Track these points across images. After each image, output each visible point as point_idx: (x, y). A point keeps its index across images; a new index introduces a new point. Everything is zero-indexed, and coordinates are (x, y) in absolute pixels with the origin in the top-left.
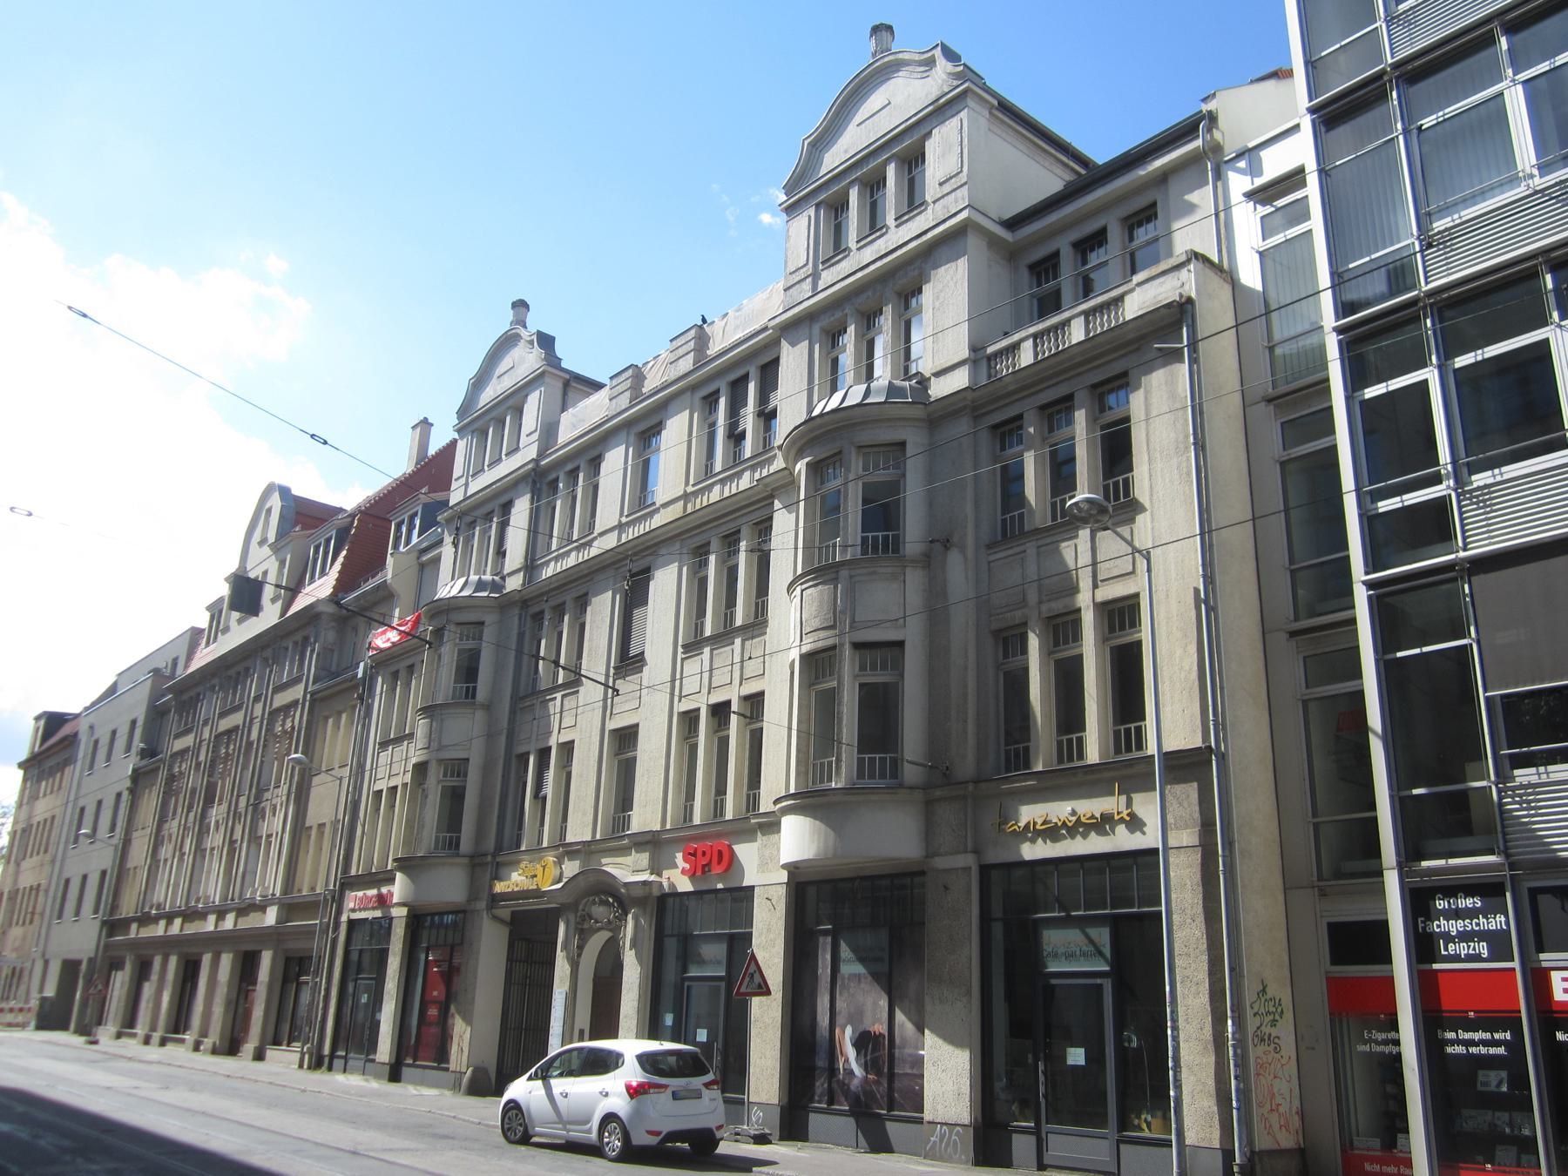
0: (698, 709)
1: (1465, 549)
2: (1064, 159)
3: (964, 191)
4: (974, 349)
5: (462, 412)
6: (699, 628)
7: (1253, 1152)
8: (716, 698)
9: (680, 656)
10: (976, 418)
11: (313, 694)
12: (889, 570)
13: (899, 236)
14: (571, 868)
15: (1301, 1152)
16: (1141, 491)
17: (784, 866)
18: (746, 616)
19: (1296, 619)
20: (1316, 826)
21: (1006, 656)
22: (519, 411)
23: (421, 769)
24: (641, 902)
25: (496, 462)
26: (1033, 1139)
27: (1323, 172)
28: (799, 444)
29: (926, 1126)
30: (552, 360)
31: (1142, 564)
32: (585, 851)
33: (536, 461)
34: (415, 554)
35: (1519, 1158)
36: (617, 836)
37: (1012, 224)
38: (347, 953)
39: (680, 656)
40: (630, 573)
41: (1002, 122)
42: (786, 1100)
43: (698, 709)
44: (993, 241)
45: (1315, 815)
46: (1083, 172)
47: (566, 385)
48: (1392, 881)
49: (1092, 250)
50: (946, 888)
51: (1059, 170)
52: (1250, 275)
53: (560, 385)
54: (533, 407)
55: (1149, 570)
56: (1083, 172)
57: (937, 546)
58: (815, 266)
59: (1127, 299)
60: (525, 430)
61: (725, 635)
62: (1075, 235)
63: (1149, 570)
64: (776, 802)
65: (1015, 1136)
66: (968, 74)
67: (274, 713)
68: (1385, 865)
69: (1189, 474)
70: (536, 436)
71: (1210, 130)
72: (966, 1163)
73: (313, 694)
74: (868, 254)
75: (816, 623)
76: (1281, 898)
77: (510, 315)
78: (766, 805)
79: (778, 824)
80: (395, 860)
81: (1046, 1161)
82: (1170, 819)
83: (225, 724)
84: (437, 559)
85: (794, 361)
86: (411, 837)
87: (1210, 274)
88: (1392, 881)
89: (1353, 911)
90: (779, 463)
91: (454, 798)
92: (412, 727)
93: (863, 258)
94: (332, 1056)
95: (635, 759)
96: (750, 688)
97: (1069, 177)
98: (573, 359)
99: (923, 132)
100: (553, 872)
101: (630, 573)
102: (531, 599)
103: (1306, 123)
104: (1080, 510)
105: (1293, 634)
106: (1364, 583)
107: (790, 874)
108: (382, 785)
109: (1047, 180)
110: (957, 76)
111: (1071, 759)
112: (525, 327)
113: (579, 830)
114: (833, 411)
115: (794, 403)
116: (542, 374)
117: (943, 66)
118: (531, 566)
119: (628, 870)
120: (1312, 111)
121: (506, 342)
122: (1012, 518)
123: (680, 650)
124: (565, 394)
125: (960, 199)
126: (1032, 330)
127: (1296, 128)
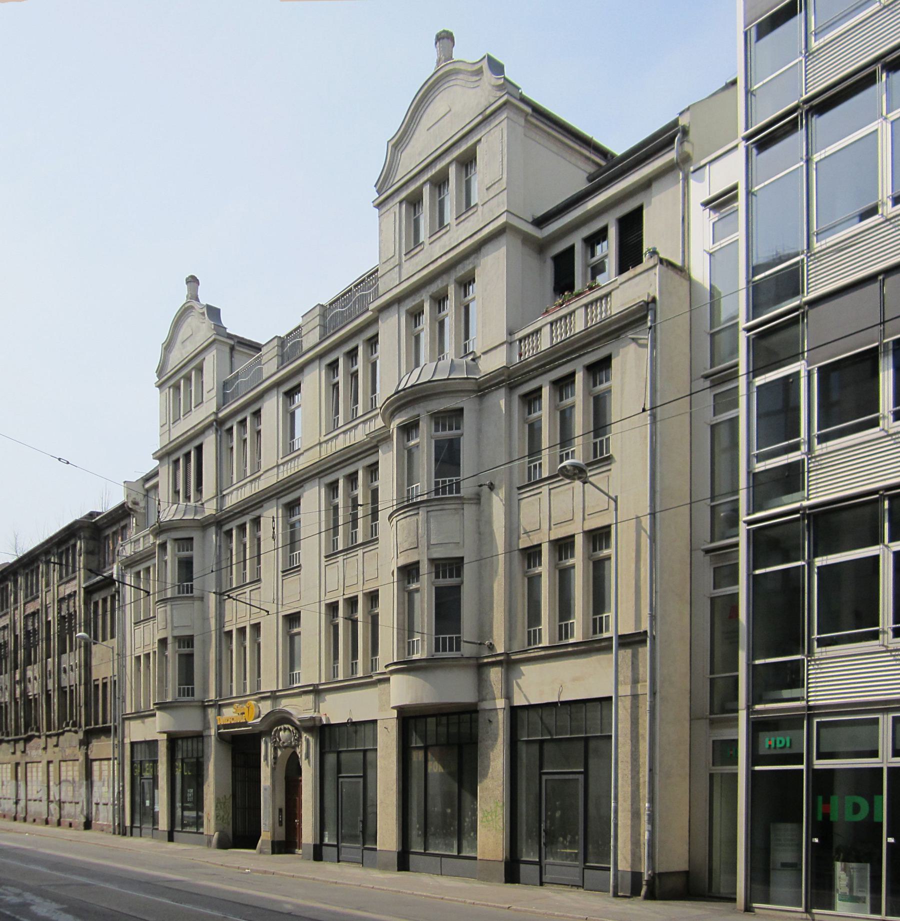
0: (338, 602)
1: (808, 499)
2: (587, 153)
3: (504, 195)
4: (510, 333)
5: (160, 371)
6: (335, 543)
7: (654, 873)
8: (349, 594)
9: (323, 564)
10: (511, 388)
11: (85, 588)
12: (453, 506)
13: (460, 234)
14: (266, 707)
15: (687, 873)
16: (614, 450)
17: (393, 708)
18: (365, 535)
19: (712, 541)
20: (712, 681)
21: (529, 567)
22: (200, 369)
23: (163, 642)
24: (309, 730)
25: (188, 411)
26: (538, 867)
27: (749, 193)
28: (391, 409)
29: (478, 862)
30: (219, 328)
31: (612, 503)
32: (274, 696)
33: (216, 414)
34: (141, 483)
35: (164, 732)
36: (291, 688)
37: (540, 222)
38: (132, 763)
39: (323, 564)
40: (287, 496)
41: (537, 127)
42: (400, 848)
43: (338, 602)
44: (527, 239)
45: (712, 672)
46: (603, 163)
47: (232, 349)
48: (742, 715)
49: (598, 243)
50: (490, 721)
51: (581, 163)
52: (700, 271)
53: (227, 350)
54: (210, 361)
55: (616, 509)
56: (603, 163)
57: (486, 489)
58: (400, 257)
59: (613, 293)
60: (206, 388)
61: (350, 549)
62: (587, 231)
63: (616, 509)
64: (386, 666)
65: (522, 866)
66: (508, 86)
67: (61, 601)
68: (740, 707)
69: (646, 438)
70: (214, 393)
71: (681, 143)
72: (500, 882)
73: (85, 588)
74: (438, 249)
75: (406, 546)
76: (687, 725)
77: (184, 290)
78: (381, 669)
79: (388, 680)
80: (154, 704)
81: (544, 880)
82: (621, 678)
83: (31, 609)
84: (156, 486)
85: (391, 329)
86: (163, 690)
87: (671, 273)
88: (742, 715)
89: (725, 734)
90: (379, 423)
91: (187, 663)
92: (154, 612)
93: (436, 251)
94: (132, 827)
95: (609, 391)
96: (370, 587)
97: (591, 169)
98: (234, 326)
99: (475, 139)
100: (254, 711)
101: (287, 496)
102: (223, 520)
103: (742, 145)
104: (567, 470)
105: (707, 551)
106: (745, 522)
107: (168, 736)
108: (140, 652)
109: (572, 176)
110: (500, 88)
111: (535, 643)
112: (197, 300)
113: (269, 684)
114: (412, 386)
115: (392, 372)
116: (214, 341)
117: (489, 77)
118: (220, 496)
119: (300, 708)
120: (747, 138)
121: (184, 313)
122: (535, 466)
123: (323, 559)
124: (232, 357)
125: (500, 205)
126: (550, 318)
127: (736, 147)
